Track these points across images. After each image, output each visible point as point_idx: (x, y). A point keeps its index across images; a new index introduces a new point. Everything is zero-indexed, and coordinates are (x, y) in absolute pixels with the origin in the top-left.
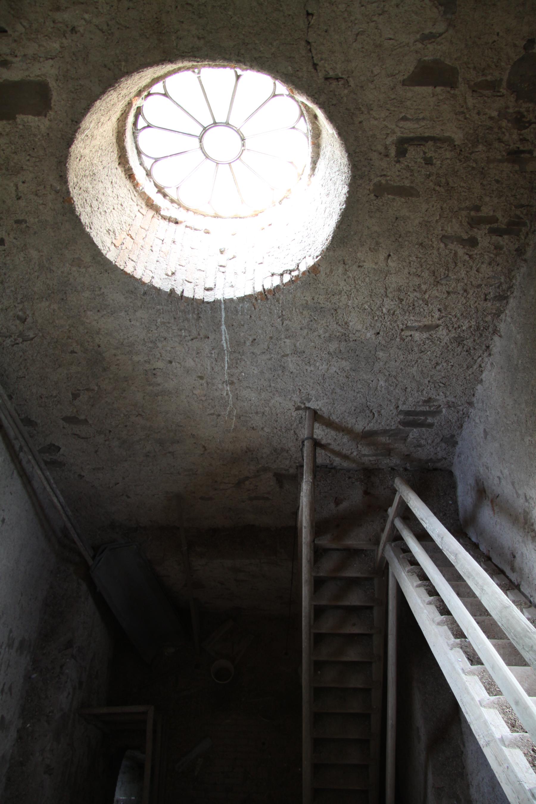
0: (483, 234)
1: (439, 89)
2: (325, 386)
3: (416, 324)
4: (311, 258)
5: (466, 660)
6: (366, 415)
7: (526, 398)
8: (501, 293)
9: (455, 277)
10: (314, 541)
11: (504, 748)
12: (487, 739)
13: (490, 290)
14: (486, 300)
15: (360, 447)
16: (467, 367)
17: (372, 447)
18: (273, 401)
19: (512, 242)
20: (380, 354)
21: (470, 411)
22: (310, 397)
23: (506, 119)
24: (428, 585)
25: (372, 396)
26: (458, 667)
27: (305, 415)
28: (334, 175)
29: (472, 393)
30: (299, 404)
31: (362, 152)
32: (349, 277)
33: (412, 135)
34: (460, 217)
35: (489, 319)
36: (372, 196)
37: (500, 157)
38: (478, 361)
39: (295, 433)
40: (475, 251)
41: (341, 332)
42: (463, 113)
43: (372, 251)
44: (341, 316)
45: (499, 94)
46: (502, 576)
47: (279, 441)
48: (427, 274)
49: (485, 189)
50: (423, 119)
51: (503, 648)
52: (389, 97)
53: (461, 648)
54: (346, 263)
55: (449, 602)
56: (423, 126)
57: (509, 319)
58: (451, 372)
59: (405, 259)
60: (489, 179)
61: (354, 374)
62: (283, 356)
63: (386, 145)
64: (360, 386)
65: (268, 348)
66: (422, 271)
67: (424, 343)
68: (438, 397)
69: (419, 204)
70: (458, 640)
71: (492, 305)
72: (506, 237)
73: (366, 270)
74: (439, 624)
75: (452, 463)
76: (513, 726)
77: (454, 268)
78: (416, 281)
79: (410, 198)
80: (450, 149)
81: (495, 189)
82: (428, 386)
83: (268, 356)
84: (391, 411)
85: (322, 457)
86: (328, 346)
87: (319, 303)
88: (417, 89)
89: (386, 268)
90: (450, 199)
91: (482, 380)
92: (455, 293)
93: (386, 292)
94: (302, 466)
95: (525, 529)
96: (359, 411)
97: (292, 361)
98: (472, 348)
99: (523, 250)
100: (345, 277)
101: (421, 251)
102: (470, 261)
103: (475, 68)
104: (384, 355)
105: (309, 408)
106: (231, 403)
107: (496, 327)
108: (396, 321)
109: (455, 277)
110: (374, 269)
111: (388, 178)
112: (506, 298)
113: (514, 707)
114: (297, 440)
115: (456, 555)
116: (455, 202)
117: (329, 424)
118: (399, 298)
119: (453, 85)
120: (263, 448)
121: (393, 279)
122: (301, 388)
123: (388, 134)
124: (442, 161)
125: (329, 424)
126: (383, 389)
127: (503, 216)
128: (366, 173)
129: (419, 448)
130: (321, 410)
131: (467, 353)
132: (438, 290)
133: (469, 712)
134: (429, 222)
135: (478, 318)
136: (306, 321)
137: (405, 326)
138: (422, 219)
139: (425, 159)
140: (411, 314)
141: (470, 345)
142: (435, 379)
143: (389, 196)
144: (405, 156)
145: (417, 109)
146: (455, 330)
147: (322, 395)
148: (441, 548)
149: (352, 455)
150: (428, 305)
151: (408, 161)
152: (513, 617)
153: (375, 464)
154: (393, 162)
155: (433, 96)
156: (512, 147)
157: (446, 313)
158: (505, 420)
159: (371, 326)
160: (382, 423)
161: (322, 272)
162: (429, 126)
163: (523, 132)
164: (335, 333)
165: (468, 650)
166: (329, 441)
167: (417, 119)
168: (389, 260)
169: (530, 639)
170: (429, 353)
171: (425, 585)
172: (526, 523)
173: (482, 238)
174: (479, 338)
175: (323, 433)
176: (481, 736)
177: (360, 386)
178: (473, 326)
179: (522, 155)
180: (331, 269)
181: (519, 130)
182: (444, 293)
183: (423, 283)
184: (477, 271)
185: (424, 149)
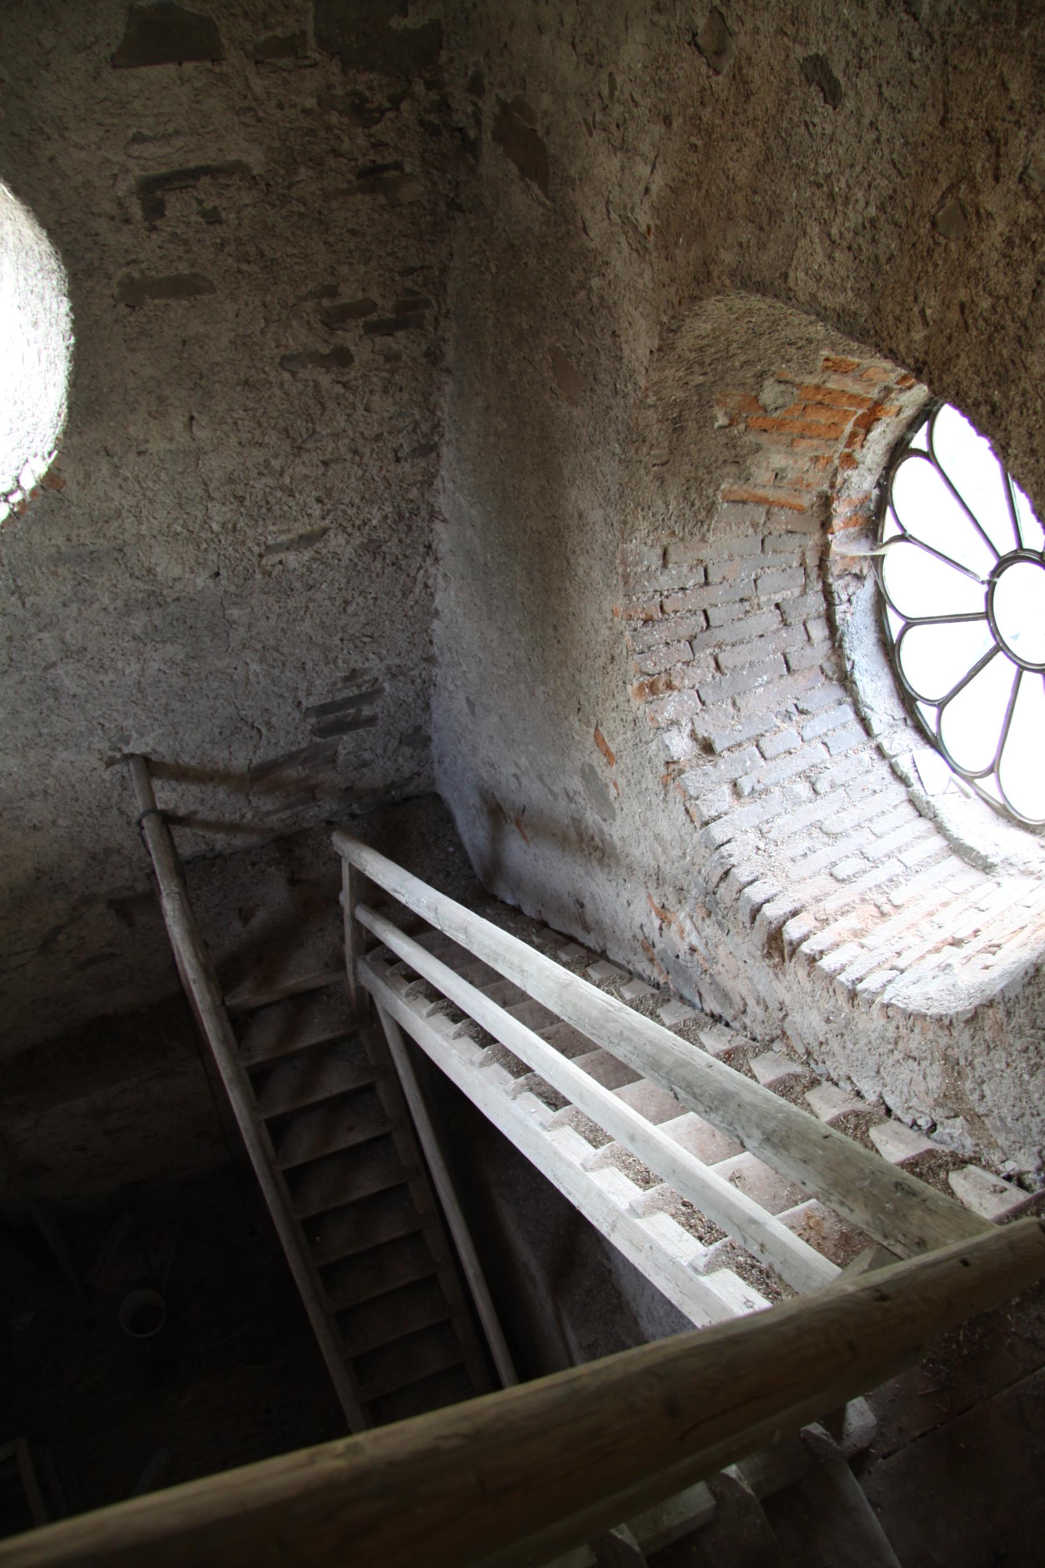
0: (357, 339)
1: (189, 67)
2: (147, 703)
3: (283, 538)
4: (39, 458)
5: (544, 1106)
6: (244, 737)
7: (517, 619)
8: (422, 441)
9: (329, 430)
10: (223, 1003)
11: (637, 1221)
12: (610, 1220)
13: (402, 441)
14: (398, 460)
15: (254, 800)
16: (404, 594)
17: (278, 794)
18: (56, 763)
19: (414, 342)
20: (235, 612)
21: (434, 673)
22: (126, 733)
23: (334, 109)
24: (448, 1006)
25: (244, 697)
26: (533, 1124)
27: (129, 770)
28: (35, 282)
29: (428, 639)
30: (110, 753)
31: (73, 222)
32: (126, 479)
33: (164, 170)
34: (304, 315)
35: (414, 493)
36: (122, 308)
37: (345, 186)
38: (420, 577)
39: (122, 812)
40: (352, 374)
41: (144, 591)
42: (250, 109)
43: (156, 418)
44: (134, 560)
45: (306, 62)
46: (572, 946)
47: (96, 837)
48: (274, 437)
49: (334, 252)
50: (177, 133)
51: (602, 1064)
52: (93, 97)
53: (531, 1090)
54: (111, 452)
55: (483, 1017)
56: (182, 148)
57: (450, 486)
58: (377, 611)
59: (223, 418)
60: (337, 231)
61: (196, 665)
62: (46, 669)
63: (119, 198)
64: (215, 685)
65: (11, 660)
66: (264, 434)
67: (310, 570)
68: (367, 665)
69: (217, 305)
70: (522, 1079)
71: (413, 466)
72: (400, 334)
73: (156, 457)
74: (482, 1065)
75: (434, 779)
76: (646, 1181)
77: (322, 414)
78: (258, 455)
79: (198, 297)
80: (247, 185)
81: (352, 248)
82: (342, 649)
83: (17, 677)
84: (289, 714)
85: (188, 843)
86: (129, 624)
87: (84, 545)
88: (146, 71)
89: (194, 445)
90: (276, 283)
91: (437, 610)
92: (336, 461)
93: (207, 491)
94: (154, 872)
95: (584, 850)
96: (228, 732)
97: (67, 673)
98: (400, 557)
99: (438, 352)
100: (119, 480)
101: (251, 396)
102: (348, 394)
103: (246, 15)
104: (240, 612)
105: (132, 755)
107: (433, 506)
108: (243, 541)
109: (329, 430)
110: (170, 450)
111: (144, 266)
112: (434, 448)
113: (631, 1148)
114: (129, 823)
115: (465, 930)
116: (287, 287)
117: (181, 774)
118: (235, 497)
119: (214, 55)
120: (69, 861)
121: (212, 462)
122: (102, 721)
123: (116, 175)
124: (238, 213)
125: (181, 774)
126: (261, 677)
127: (383, 296)
128: (97, 264)
129: (364, 770)
130: (155, 751)
131: (395, 568)
132: (304, 463)
133: (572, 1190)
134: (249, 336)
135: (394, 497)
136: (69, 587)
137: (263, 547)
138: (233, 334)
139: (204, 214)
140: (269, 522)
141: (395, 550)
142: (351, 631)
143: (157, 301)
144: (163, 215)
145: (157, 115)
146: (359, 529)
147: (148, 722)
148: (439, 928)
149: (245, 821)
150: (294, 496)
151: (173, 224)
152: (581, 997)
153: (294, 823)
154: (142, 230)
155: (182, 84)
156: (362, 161)
157: (332, 502)
158: (494, 670)
159: (199, 564)
160: (281, 743)
161: (69, 483)
162: (192, 147)
163: (375, 129)
164: (133, 595)
165: (544, 1089)
166: (192, 808)
167: (164, 135)
168: (194, 429)
169: (616, 1021)
170: (324, 586)
171: (442, 1008)
172: (582, 840)
173: (356, 345)
174: (407, 535)
175: (174, 796)
176: (601, 1220)
177: (215, 685)
178: (390, 515)
179: (386, 175)
180: (86, 470)
181: (364, 127)
182: (317, 466)
183: (272, 456)
184: (367, 409)
185: (195, 194)
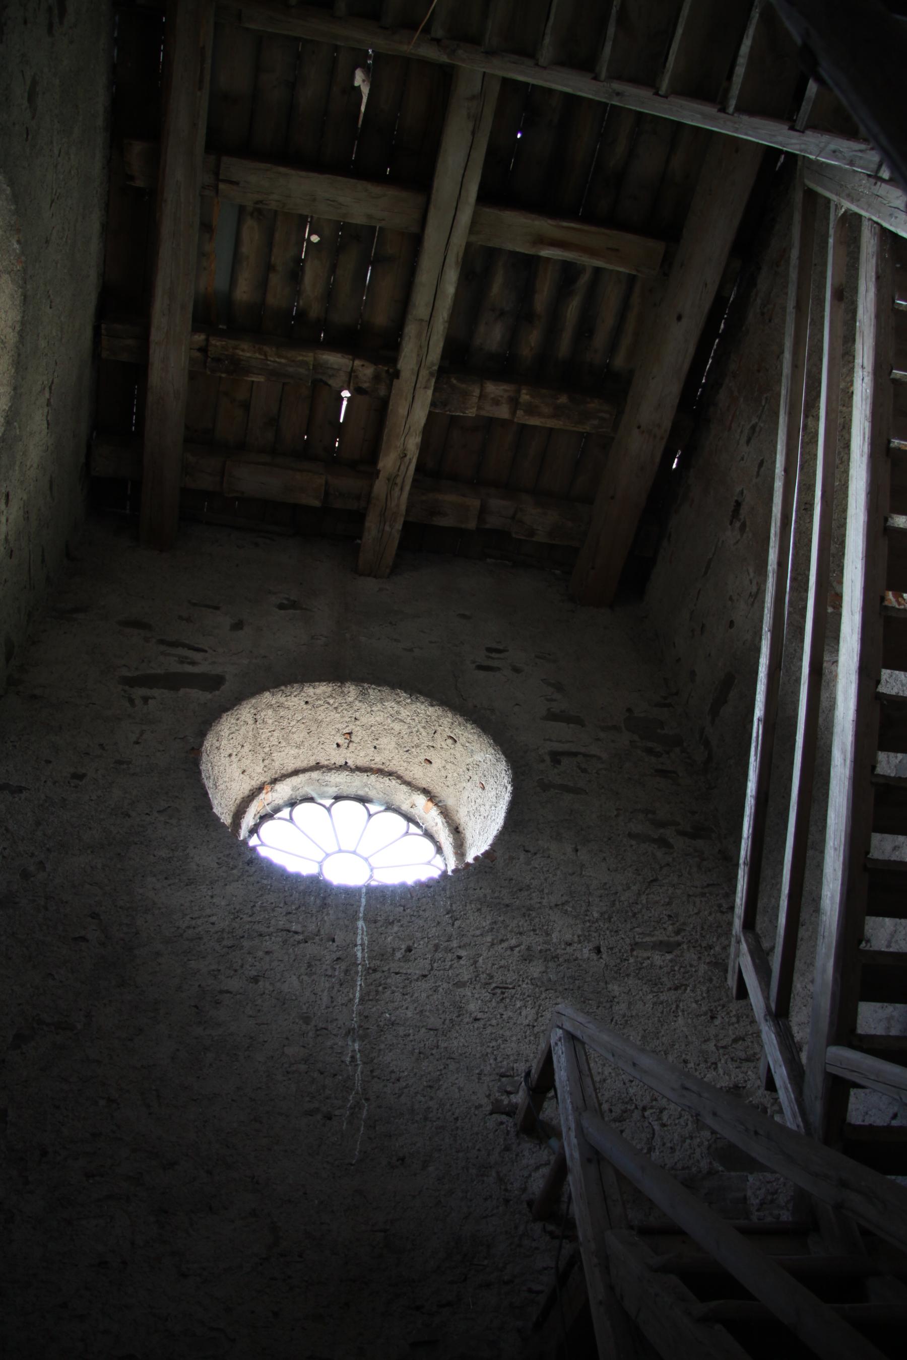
106: (358, 1086)
